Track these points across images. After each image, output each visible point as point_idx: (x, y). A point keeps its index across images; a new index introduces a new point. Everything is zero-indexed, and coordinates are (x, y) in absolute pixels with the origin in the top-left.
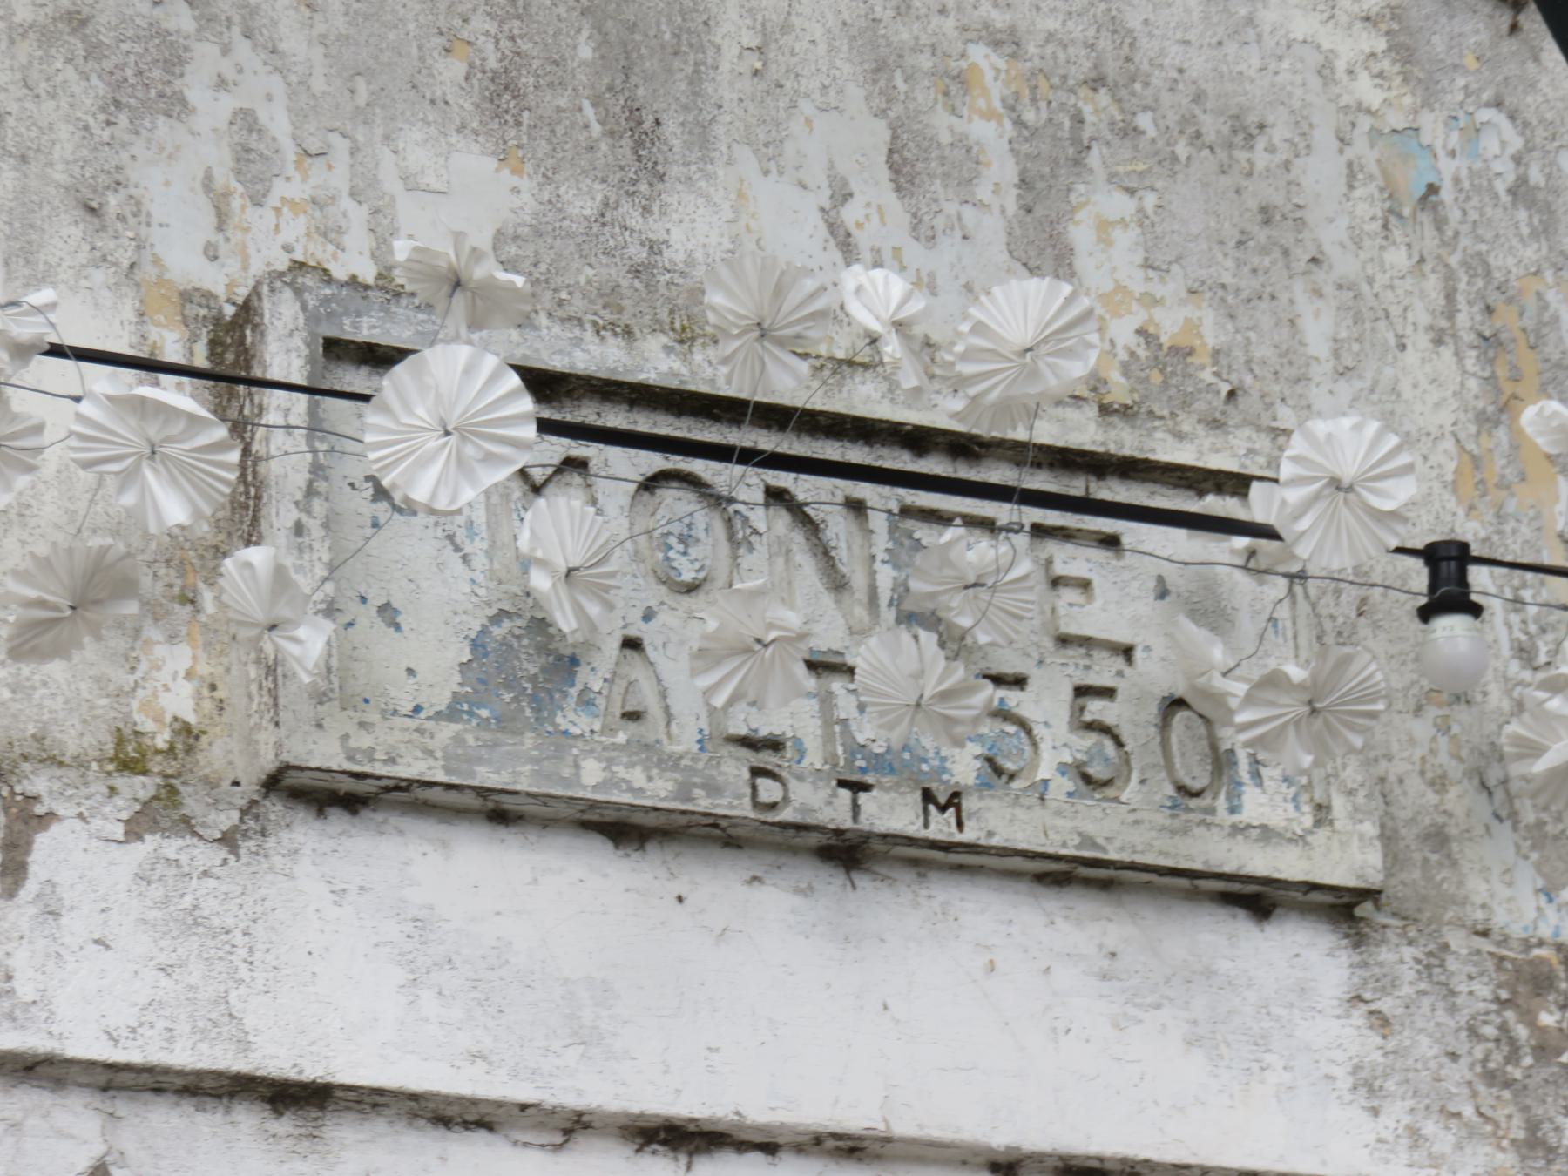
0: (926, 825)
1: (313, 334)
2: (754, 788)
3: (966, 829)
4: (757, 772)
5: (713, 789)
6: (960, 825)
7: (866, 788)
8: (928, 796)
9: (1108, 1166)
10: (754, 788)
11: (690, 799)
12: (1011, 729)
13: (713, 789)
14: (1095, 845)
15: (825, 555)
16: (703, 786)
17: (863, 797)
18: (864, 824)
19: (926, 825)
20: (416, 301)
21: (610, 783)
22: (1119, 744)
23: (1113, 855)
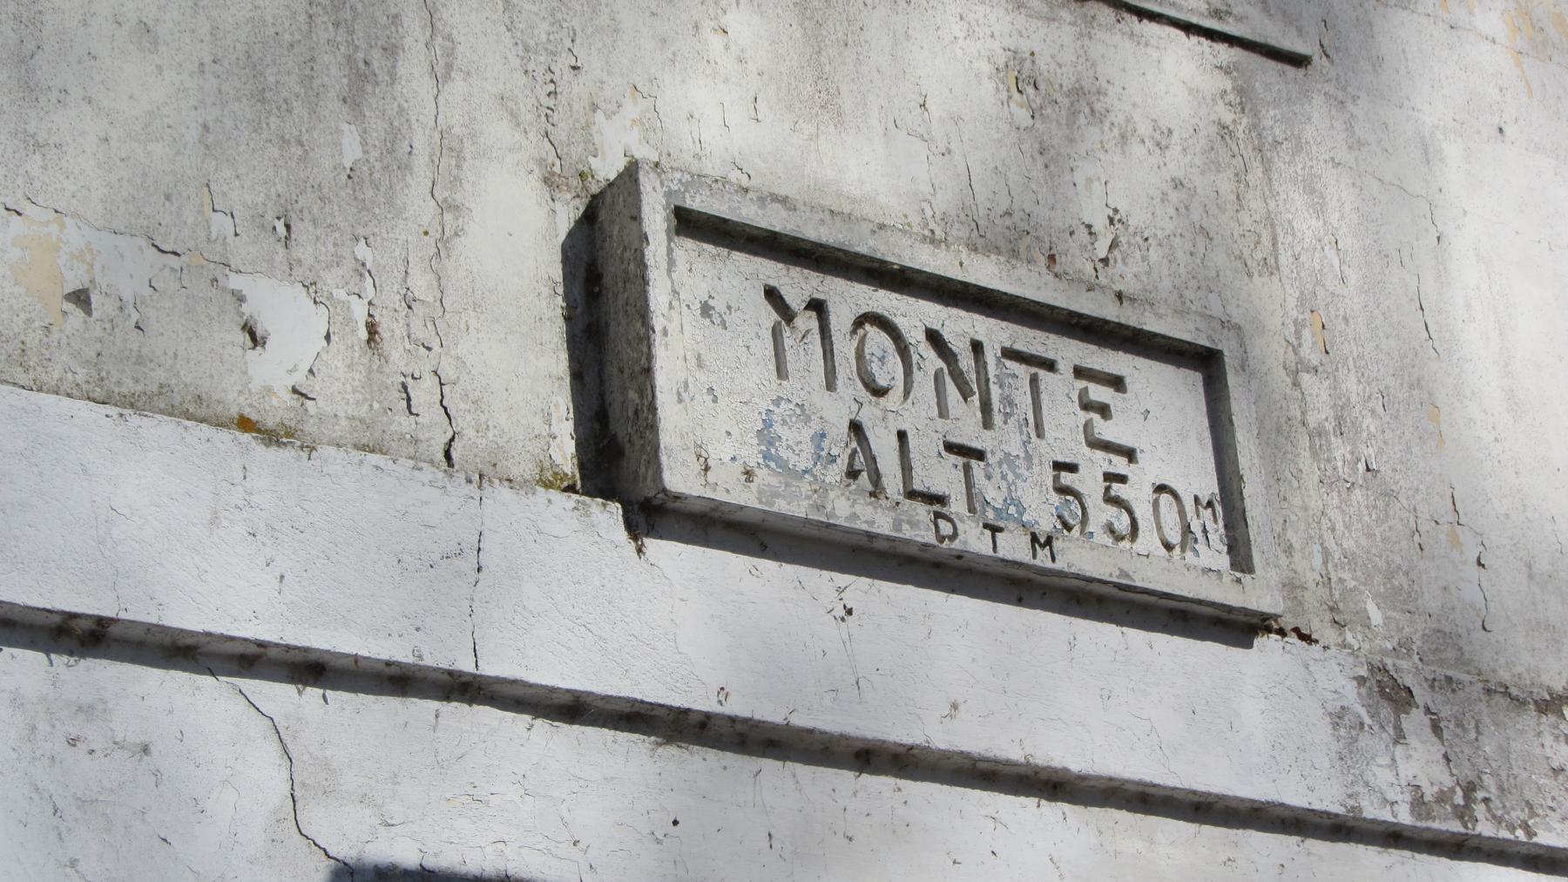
0: (1034, 556)
1: (668, 203)
2: (937, 526)
3: (1140, 540)
4: (938, 515)
5: (913, 524)
6: (1053, 559)
7: (1000, 530)
8: (1034, 538)
9: (1127, 786)
10: (937, 526)
11: (900, 530)
12: (1070, 498)
13: (913, 524)
14: (1128, 576)
15: (828, 354)
16: (909, 522)
17: (998, 535)
18: (1001, 554)
19: (1034, 556)
20: (550, 128)
21: (854, 516)
22: (1130, 512)
23: (1139, 584)
